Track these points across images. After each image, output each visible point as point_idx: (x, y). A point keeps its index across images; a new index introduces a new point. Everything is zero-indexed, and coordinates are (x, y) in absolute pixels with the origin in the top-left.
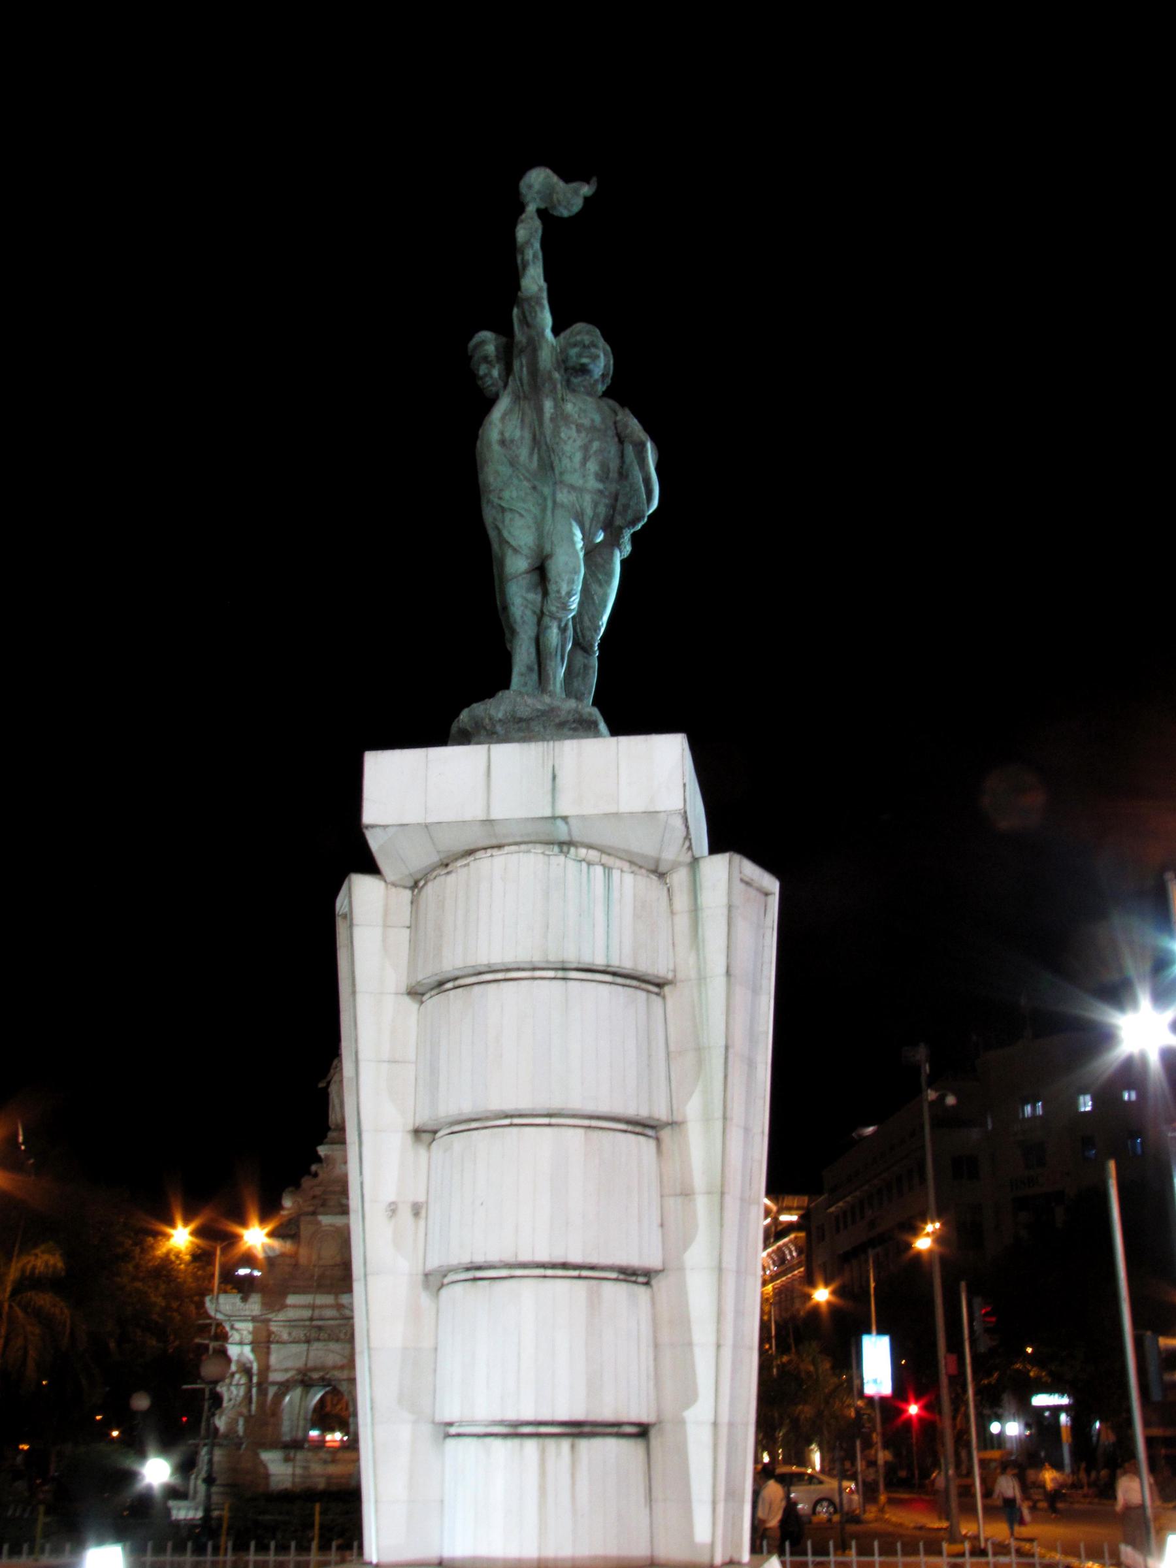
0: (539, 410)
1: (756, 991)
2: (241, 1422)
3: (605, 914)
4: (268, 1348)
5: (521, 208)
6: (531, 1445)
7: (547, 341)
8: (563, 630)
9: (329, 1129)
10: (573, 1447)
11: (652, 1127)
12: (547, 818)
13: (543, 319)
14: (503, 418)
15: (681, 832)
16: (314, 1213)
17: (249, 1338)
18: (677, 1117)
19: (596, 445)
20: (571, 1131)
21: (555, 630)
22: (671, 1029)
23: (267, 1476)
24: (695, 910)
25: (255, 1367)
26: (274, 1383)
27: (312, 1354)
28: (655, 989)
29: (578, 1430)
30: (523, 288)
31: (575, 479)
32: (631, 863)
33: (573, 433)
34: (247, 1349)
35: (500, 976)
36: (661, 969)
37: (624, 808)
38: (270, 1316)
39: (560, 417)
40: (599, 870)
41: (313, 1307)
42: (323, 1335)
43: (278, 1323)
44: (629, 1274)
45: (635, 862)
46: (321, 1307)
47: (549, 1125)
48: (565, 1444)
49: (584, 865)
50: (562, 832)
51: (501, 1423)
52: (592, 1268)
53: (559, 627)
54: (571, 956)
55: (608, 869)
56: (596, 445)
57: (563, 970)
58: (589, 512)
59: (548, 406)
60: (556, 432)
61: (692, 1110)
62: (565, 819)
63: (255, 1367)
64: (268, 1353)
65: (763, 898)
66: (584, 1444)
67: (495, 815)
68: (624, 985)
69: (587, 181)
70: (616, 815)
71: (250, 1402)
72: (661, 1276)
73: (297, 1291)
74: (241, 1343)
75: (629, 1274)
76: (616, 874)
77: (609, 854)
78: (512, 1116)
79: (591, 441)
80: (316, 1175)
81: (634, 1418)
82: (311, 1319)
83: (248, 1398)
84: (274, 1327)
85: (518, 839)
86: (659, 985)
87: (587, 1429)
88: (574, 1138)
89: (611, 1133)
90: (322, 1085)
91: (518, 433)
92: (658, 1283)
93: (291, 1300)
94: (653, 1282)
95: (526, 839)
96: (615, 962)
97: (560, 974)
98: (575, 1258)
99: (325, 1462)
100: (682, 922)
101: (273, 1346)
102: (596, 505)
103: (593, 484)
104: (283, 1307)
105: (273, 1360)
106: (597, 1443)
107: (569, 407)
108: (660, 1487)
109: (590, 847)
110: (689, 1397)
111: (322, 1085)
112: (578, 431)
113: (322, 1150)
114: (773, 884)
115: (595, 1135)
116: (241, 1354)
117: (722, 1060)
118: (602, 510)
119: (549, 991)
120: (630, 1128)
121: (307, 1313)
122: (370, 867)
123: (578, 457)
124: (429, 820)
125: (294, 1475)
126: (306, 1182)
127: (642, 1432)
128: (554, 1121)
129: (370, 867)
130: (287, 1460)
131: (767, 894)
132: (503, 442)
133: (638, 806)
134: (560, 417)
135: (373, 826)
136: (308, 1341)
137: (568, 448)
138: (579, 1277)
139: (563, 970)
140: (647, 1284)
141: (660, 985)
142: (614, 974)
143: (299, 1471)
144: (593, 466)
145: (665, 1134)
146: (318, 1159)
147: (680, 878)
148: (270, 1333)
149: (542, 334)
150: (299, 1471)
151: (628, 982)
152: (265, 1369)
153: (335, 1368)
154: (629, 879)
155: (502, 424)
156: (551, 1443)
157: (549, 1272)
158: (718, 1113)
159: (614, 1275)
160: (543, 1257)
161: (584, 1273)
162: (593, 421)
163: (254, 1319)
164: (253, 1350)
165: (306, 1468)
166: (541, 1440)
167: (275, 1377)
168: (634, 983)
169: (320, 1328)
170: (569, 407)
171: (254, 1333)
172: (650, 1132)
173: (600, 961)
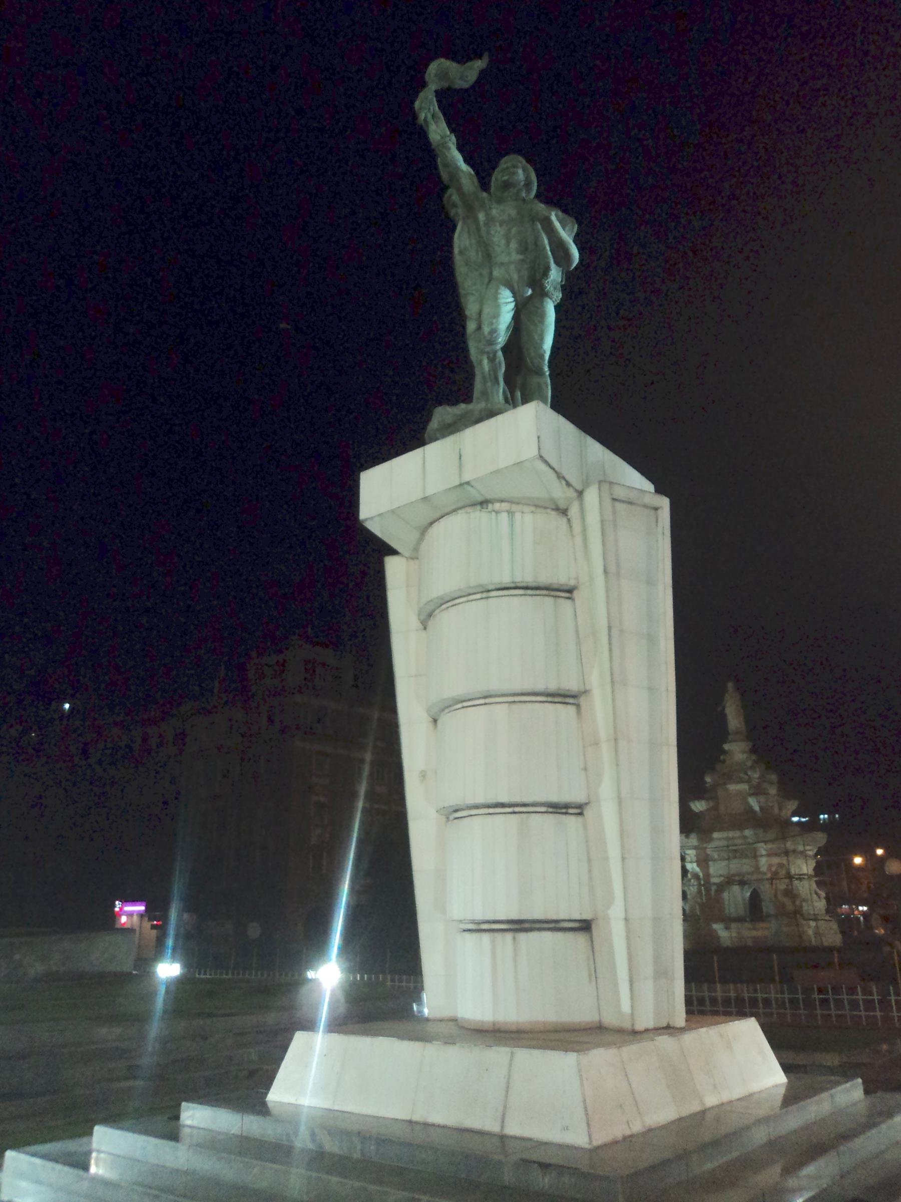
0: (476, 220)
1: (650, 582)
2: (697, 907)
3: (512, 544)
4: (707, 864)
5: (423, 85)
6: (486, 937)
7: (462, 171)
8: (492, 359)
9: (728, 733)
10: (514, 938)
11: (574, 697)
12: (456, 487)
13: (453, 157)
14: (459, 236)
15: (553, 475)
16: (725, 784)
17: (695, 859)
18: (587, 688)
19: (514, 230)
20: (499, 706)
21: (485, 361)
22: (580, 621)
23: (719, 938)
24: (584, 531)
25: (701, 875)
26: (715, 884)
27: (731, 866)
28: (567, 595)
29: (519, 926)
30: (432, 141)
31: (504, 259)
32: (536, 506)
33: (498, 228)
34: (695, 864)
35: (450, 604)
36: (562, 578)
37: (502, 465)
38: (705, 845)
39: (490, 220)
40: (504, 516)
41: (728, 839)
42: (738, 855)
43: (710, 849)
44: (558, 808)
45: (538, 505)
46: (733, 838)
47: (485, 704)
48: (509, 936)
49: (494, 514)
50: (473, 494)
51: (473, 922)
52: (524, 805)
53: (488, 358)
54: (486, 579)
55: (511, 513)
56: (514, 230)
57: (486, 591)
58: (515, 277)
59: (481, 216)
60: (488, 233)
61: (597, 681)
62: (468, 483)
63: (701, 875)
64: (708, 867)
65: (652, 512)
66: (522, 936)
67: (429, 493)
68: (532, 595)
69: (480, 56)
70: (498, 472)
71: (701, 896)
72: (588, 807)
73: (721, 830)
74: (691, 862)
75: (558, 808)
76: (518, 516)
77: (518, 503)
78: (463, 701)
79: (509, 230)
80: (724, 762)
81: (577, 917)
82: (728, 846)
83: (700, 892)
84: (709, 851)
85: (454, 507)
86: (569, 591)
87: (527, 925)
88: (500, 711)
89: (529, 705)
90: (719, 709)
91: (467, 243)
92: (588, 812)
93: (716, 835)
94: (585, 813)
95: (460, 505)
96: (518, 579)
97: (485, 595)
98: (504, 799)
99: (749, 929)
100: (578, 540)
101: (711, 863)
102: (519, 271)
103: (516, 257)
104: (711, 840)
105: (712, 870)
106: (534, 936)
107: (494, 212)
108: (596, 969)
109: (502, 501)
110: (610, 903)
111: (719, 709)
112: (501, 225)
113: (726, 747)
114: (665, 503)
115: (514, 706)
116: (693, 868)
117: (607, 637)
118: (525, 273)
119: (475, 608)
120: (550, 699)
121: (725, 843)
122: (393, 552)
123: (503, 242)
124: (394, 507)
125: (731, 937)
126: (718, 766)
127: (585, 926)
128: (487, 701)
129: (393, 552)
130: (727, 928)
131: (656, 509)
132: (461, 253)
133: (510, 462)
134: (490, 220)
135: (366, 520)
136: (728, 859)
137: (495, 239)
138: (514, 813)
139: (486, 591)
140: (581, 814)
141: (570, 591)
142: (526, 588)
143: (734, 935)
144: (514, 245)
145: (582, 701)
146: (725, 752)
147: (574, 511)
148: (707, 855)
149: (457, 168)
150: (734, 935)
151: (538, 592)
152: (707, 876)
153: (748, 874)
154: (528, 518)
155: (461, 240)
156: (498, 936)
157: (491, 811)
158: (608, 680)
159: (543, 809)
160: (480, 800)
161: (517, 809)
162: (509, 215)
163: (695, 848)
164: (698, 865)
165: (738, 933)
166: (492, 934)
167: (715, 880)
168: (544, 592)
169: (735, 851)
170: (494, 212)
171: (697, 855)
172: (571, 701)
173: (506, 580)
